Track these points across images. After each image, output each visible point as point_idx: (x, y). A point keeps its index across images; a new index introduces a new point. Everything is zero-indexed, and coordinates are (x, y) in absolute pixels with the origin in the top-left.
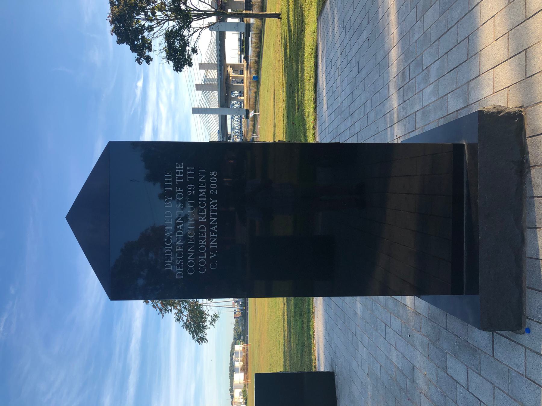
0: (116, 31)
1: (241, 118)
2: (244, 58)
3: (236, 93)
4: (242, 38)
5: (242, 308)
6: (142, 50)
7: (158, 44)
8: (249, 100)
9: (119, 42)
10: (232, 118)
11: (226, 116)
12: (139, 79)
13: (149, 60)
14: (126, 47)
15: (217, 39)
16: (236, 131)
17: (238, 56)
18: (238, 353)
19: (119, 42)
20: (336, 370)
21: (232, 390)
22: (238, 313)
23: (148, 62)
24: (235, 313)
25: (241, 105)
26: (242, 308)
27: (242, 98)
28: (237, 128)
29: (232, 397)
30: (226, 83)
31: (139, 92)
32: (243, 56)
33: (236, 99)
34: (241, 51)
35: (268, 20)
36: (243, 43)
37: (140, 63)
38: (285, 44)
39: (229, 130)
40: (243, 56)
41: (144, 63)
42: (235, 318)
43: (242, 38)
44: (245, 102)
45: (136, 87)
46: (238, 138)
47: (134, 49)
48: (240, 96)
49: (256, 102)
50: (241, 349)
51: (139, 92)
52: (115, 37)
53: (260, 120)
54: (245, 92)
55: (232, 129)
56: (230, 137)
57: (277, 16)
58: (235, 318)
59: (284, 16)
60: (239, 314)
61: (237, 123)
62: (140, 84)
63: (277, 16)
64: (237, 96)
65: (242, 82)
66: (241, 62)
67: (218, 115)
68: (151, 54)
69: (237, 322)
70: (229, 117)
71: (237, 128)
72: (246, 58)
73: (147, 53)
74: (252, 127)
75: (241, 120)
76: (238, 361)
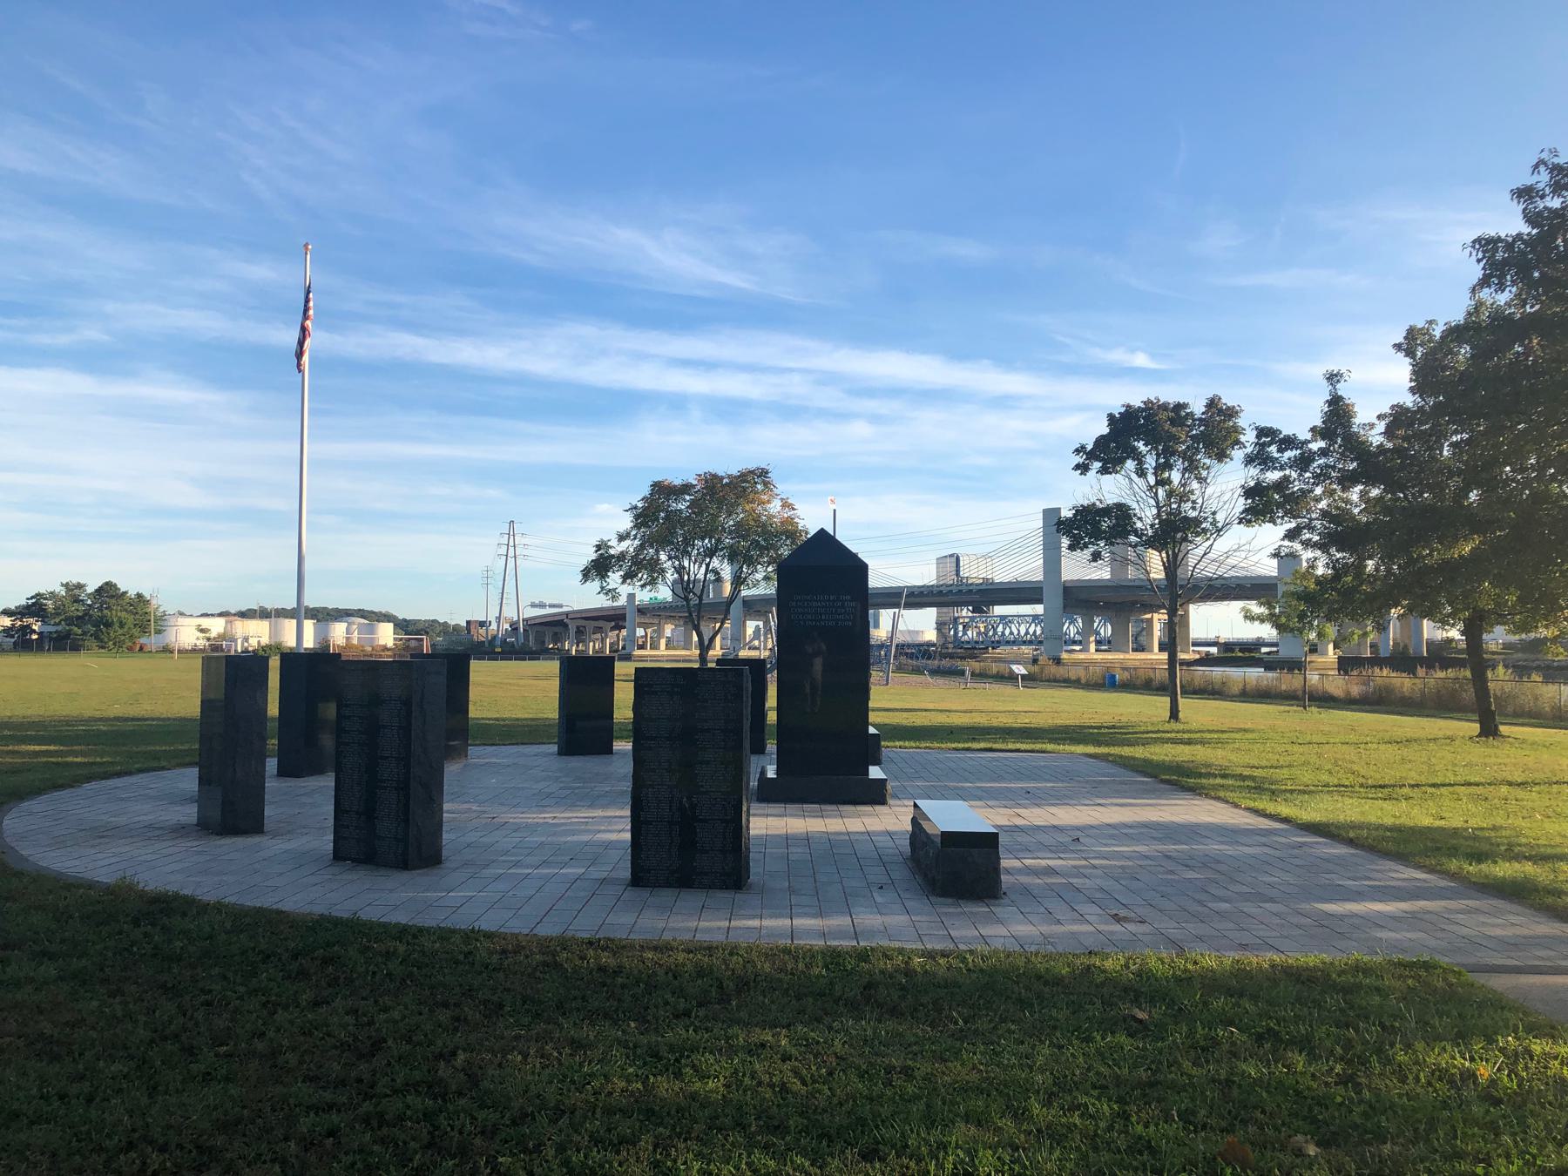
0: (1130, 414)
1: (1035, 641)
2: (1208, 654)
3: (1106, 631)
4: (1264, 650)
5: (498, 642)
6: (1108, 451)
7: (1111, 488)
8: (1086, 665)
9: (1111, 417)
10: (1035, 617)
11: (1039, 601)
12: (1153, 356)
13: (1083, 468)
14: (1103, 429)
15: (1259, 577)
16: (1000, 629)
17: (1211, 636)
18: (372, 631)
19: (1111, 417)
20: (615, 758)
21: (264, 614)
22: (482, 631)
23: (1077, 467)
24: (482, 624)
25: (1074, 642)
26: (498, 642)
27: (1093, 647)
28: (1007, 632)
29: (243, 615)
30: (1134, 603)
31: (1117, 356)
32: (1214, 650)
33: (1088, 629)
34: (1228, 647)
35: (1166, 701)
36: (1250, 651)
37: (1077, 451)
38: (1113, 727)
39: (999, 610)
40: (1214, 650)
41: (1079, 459)
42: (468, 623)
43: (1264, 650)
44: (1082, 656)
45: (1133, 351)
46: (979, 634)
47: (1101, 442)
48: (1098, 643)
49: (1055, 681)
50: (382, 642)
51: (1117, 356)
52: (1117, 410)
53: (1007, 689)
54: (1109, 656)
55: (1003, 618)
56: (982, 611)
57: (1174, 714)
58: (468, 623)
59: (1174, 726)
60: (480, 635)
61: (1027, 633)
62: (1141, 360)
63: (1174, 714)
64: (1098, 633)
65: (1140, 648)
66: (1194, 644)
67: (1041, 578)
68: (1092, 474)
69: (456, 628)
70: (1039, 609)
71: (1007, 632)
72: (1207, 660)
73: (1097, 465)
74: (995, 671)
75: (1030, 642)
76: (348, 631)
